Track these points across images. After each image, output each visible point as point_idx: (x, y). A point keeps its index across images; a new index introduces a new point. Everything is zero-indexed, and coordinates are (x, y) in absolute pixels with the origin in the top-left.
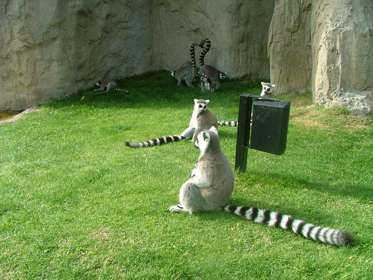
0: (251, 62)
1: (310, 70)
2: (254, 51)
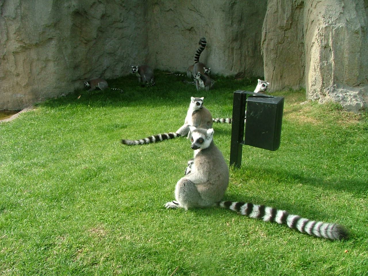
0: (245, 60)
2: (248, 48)
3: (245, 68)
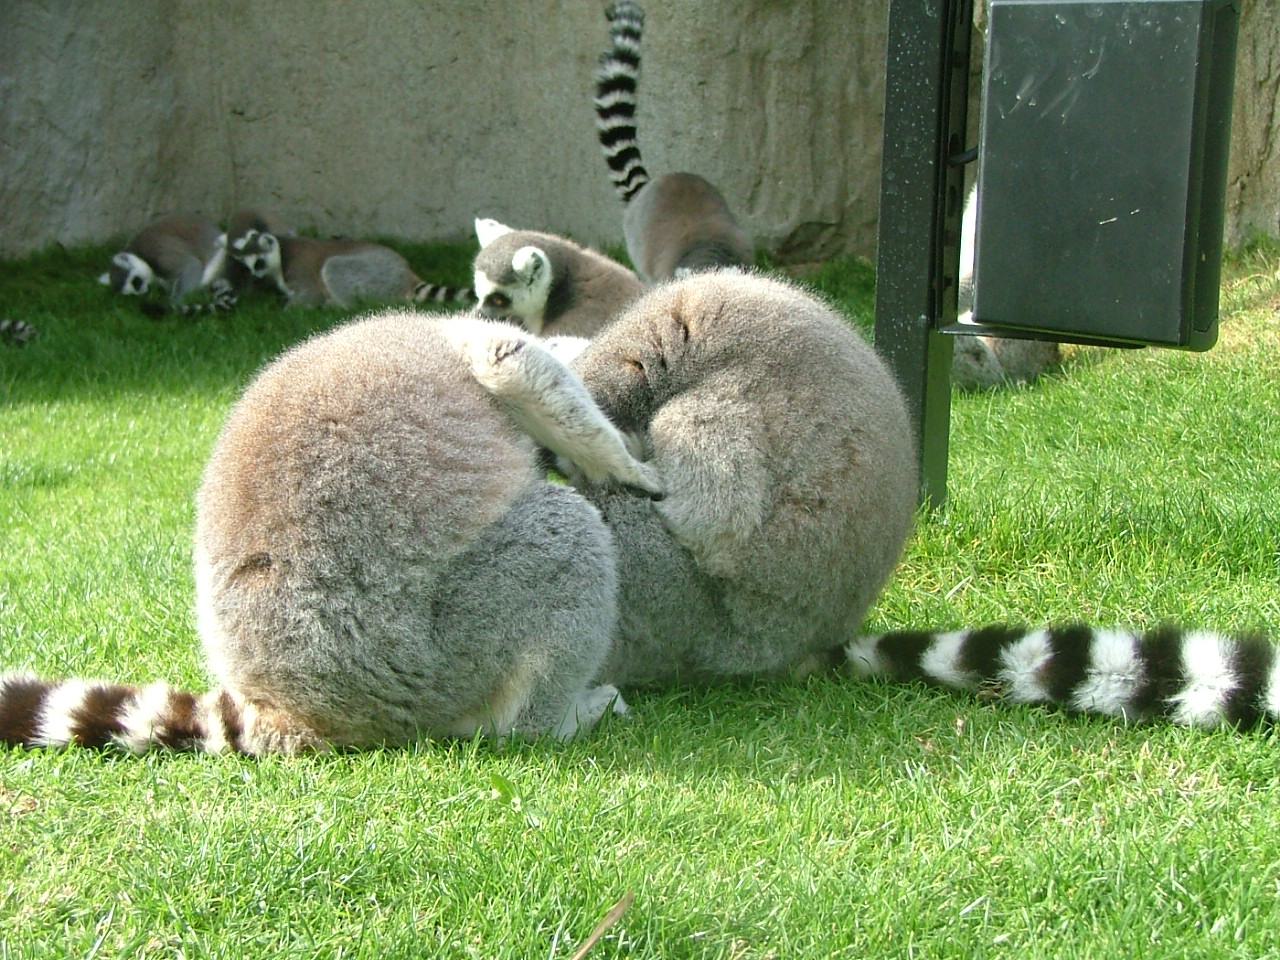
0: (843, 137)
1: (1265, 91)
2: (860, 58)
3: (843, 193)
